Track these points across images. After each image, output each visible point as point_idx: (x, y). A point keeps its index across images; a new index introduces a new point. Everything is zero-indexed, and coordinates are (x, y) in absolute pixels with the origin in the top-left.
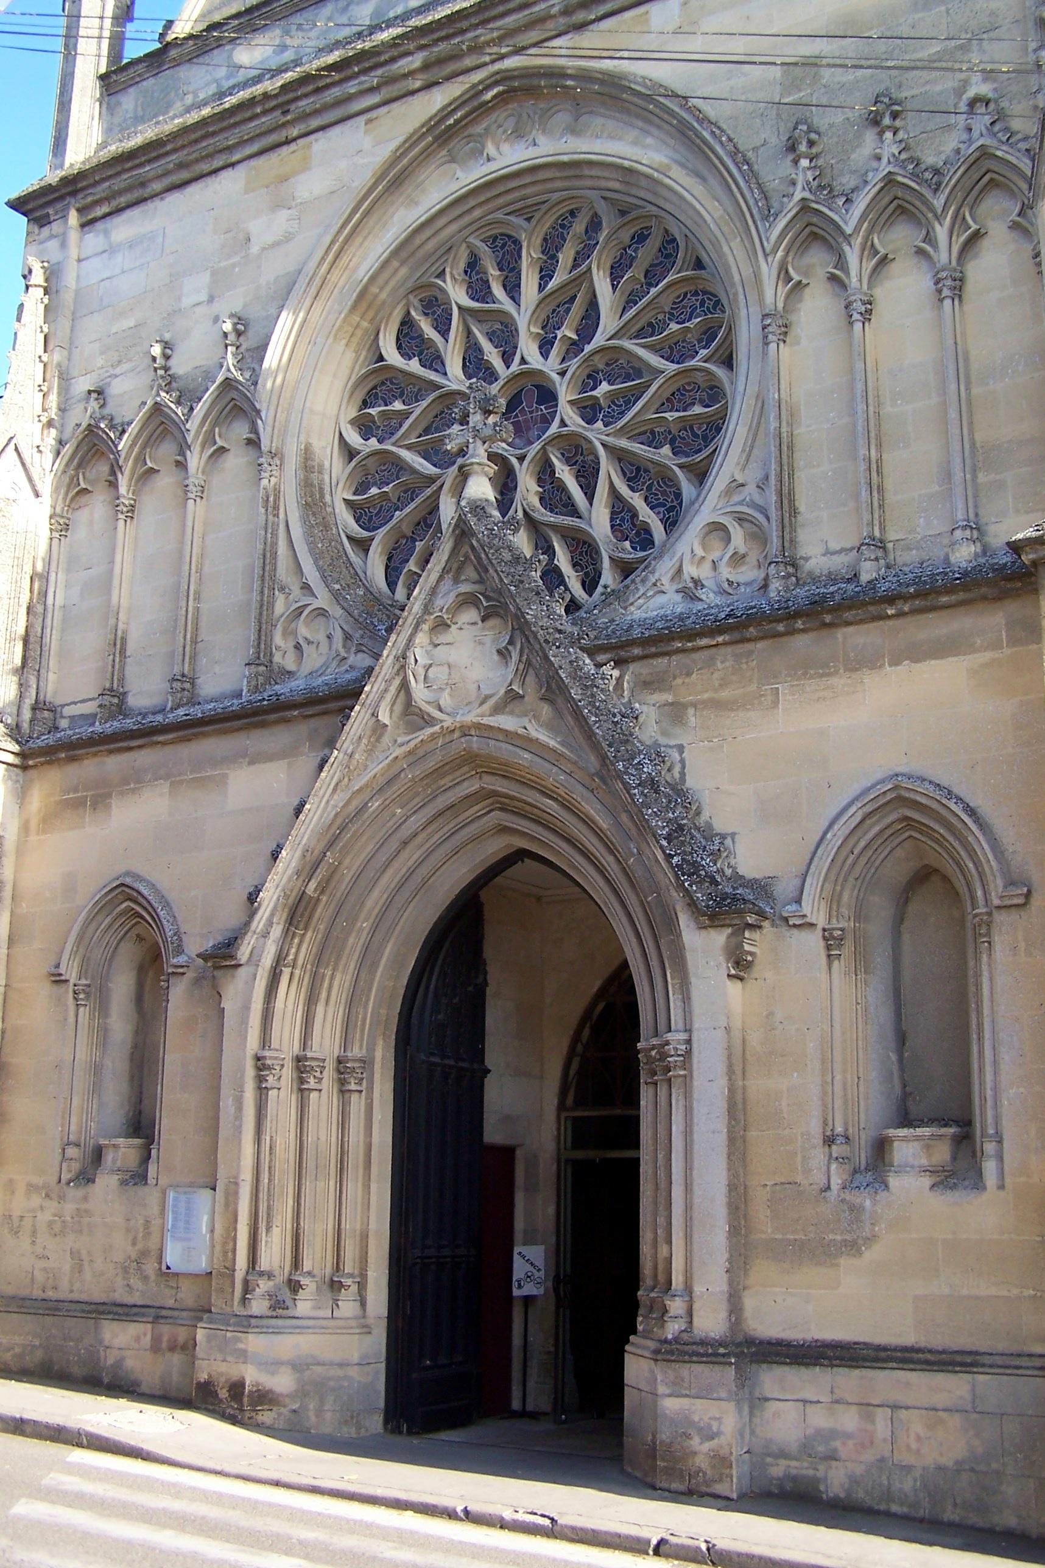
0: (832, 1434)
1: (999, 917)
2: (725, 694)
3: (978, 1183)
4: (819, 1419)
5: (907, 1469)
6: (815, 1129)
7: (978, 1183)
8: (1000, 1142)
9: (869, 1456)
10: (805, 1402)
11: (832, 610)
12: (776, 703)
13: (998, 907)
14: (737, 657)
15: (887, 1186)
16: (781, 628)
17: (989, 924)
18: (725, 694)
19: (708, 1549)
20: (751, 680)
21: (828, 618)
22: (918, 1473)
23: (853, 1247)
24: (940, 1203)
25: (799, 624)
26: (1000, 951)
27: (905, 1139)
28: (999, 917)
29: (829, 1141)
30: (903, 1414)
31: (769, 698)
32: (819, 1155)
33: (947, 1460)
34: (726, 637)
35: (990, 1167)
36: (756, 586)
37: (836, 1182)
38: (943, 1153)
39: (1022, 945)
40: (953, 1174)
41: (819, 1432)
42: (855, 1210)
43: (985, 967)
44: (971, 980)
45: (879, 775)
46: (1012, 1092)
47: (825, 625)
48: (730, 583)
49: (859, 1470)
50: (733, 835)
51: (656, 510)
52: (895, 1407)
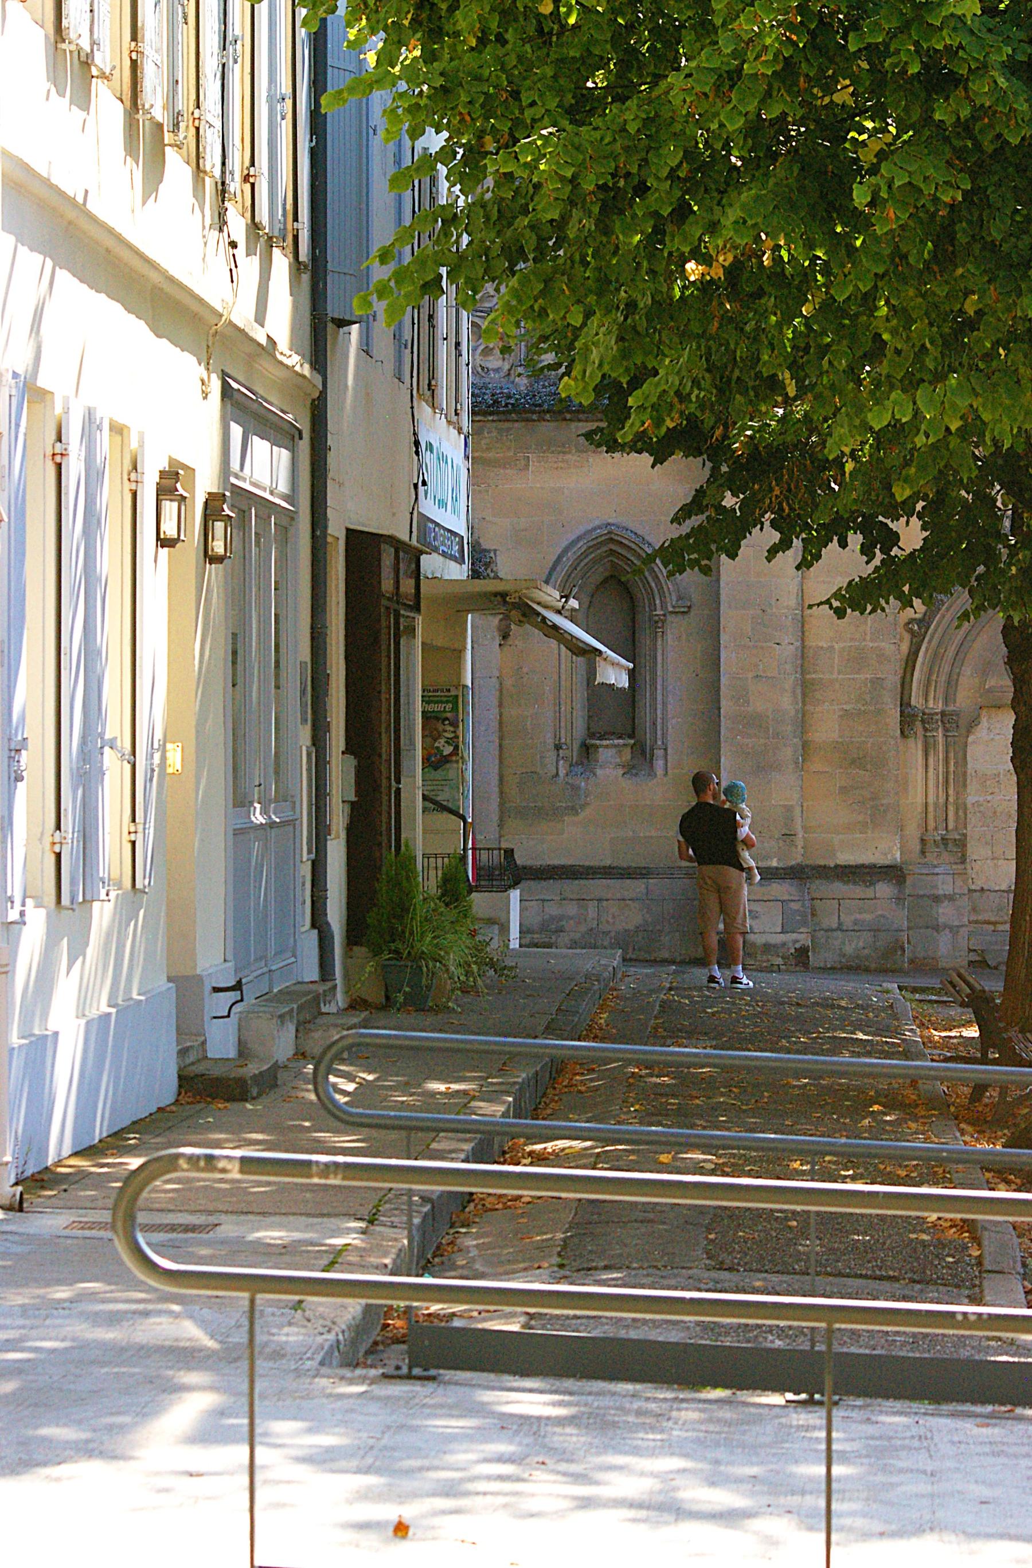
0: (561, 918)
1: (670, 618)
2: (491, 455)
3: (652, 773)
4: (553, 910)
5: (606, 933)
6: (550, 742)
7: (652, 773)
8: (666, 750)
9: (583, 928)
10: (543, 900)
11: (571, 412)
12: (527, 466)
13: (671, 612)
14: (500, 431)
15: (595, 774)
16: (535, 417)
17: (663, 622)
18: (491, 455)
19: (433, 287)
20: (509, 449)
21: (568, 416)
22: (613, 934)
23: (574, 810)
24: (626, 784)
25: (548, 416)
26: (669, 637)
27: (607, 746)
28: (670, 618)
29: (558, 747)
30: (605, 903)
31: (523, 462)
32: (551, 755)
33: (631, 927)
34: (495, 418)
35: (659, 763)
36: (502, 374)
37: (562, 772)
38: (627, 754)
39: (684, 637)
40: (634, 767)
41: (552, 918)
42: (575, 788)
43: (659, 647)
44: (998, 1158)
45: (597, 523)
46: (674, 721)
47: (565, 419)
48: (483, 368)
49: (578, 936)
50: (495, 551)
51: (427, 804)
52: (599, 900)
